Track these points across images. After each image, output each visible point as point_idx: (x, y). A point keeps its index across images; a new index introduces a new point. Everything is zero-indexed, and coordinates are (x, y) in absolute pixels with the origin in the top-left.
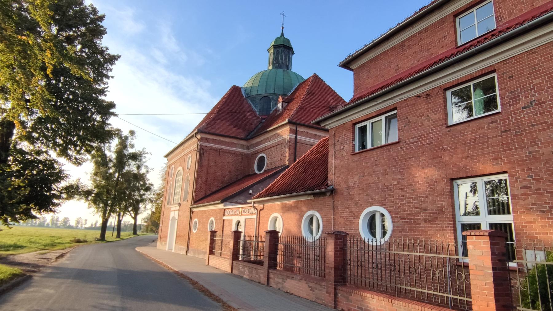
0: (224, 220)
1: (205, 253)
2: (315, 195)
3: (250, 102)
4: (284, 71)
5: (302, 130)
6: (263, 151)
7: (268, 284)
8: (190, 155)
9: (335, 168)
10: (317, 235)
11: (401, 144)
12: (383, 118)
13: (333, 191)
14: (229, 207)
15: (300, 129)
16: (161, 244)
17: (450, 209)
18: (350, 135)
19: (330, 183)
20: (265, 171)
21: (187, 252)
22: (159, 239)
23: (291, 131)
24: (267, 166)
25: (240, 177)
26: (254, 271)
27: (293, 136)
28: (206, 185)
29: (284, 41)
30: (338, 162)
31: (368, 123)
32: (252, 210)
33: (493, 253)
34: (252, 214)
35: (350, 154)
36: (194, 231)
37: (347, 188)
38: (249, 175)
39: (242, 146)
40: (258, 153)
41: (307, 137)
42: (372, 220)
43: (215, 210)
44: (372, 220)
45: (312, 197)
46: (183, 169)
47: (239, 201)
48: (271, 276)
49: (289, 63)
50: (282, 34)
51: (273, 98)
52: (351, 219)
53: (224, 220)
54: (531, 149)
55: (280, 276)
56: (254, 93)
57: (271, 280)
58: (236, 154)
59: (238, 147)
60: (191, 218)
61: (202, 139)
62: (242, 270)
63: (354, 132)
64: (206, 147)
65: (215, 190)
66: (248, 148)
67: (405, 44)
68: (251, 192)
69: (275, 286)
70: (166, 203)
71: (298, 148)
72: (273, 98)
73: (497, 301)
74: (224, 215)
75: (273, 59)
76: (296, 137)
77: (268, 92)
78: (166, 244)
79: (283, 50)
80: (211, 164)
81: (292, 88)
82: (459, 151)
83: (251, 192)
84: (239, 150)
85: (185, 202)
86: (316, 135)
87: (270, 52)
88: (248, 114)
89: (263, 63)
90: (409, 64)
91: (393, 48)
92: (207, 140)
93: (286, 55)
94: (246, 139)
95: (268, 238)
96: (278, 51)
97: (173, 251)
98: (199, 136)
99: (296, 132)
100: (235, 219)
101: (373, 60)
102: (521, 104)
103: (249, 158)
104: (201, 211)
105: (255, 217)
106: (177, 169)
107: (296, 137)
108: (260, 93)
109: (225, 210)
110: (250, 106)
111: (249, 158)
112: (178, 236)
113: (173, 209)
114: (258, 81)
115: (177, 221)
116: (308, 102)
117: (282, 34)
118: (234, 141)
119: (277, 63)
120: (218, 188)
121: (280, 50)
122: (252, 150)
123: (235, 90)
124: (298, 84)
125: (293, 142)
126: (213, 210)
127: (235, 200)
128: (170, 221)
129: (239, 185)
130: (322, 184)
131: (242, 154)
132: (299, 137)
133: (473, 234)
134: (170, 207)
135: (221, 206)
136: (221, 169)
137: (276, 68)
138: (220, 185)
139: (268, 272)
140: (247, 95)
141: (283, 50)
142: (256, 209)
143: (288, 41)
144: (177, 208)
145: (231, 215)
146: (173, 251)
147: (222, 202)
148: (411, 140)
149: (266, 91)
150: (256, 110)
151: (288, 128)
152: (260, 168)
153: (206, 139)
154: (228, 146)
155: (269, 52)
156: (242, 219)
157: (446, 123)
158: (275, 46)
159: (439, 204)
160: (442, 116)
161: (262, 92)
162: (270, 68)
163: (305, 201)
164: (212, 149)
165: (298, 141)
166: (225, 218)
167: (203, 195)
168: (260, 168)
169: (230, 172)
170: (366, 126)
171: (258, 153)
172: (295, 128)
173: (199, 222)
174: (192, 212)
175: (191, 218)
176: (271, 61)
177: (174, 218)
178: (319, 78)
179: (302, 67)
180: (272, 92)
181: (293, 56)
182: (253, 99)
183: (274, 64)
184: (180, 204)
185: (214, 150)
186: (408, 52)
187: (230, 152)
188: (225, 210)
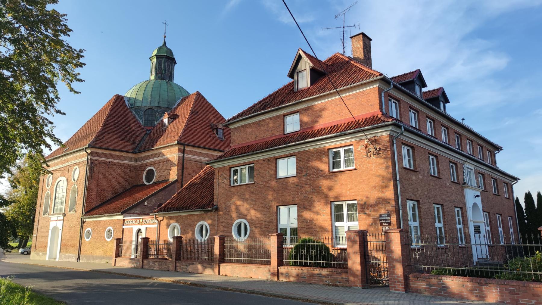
0: (123, 229)
1: (110, 258)
2: (204, 211)
3: (134, 113)
4: (167, 83)
5: (189, 149)
6: (152, 164)
7: (175, 271)
8: (76, 167)
9: (218, 194)
10: (205, 238)
11: (256, 184)
12: (247, 167)
13: (217, 209)
14: (129, 219)
15: (187, 148)
16: (38, 254)
17: (275, 221)
18: (228, 174)
19: (215, 204)
20: (154, 182)
21: (78, 259)
22: (33, 249)
23: (180, 150)
24: (156, 178)
25: (128, 188)
26: (163, 264)
27: (182, 155)
28: (97, 196)
29: (166, 52)
30: (220, 190)
31: (239, 168)
32: (153, 220)
33: (278, 242)
34: (153, 224)
35: (228, 186)
36: (86, 239)
37: (225, 207)
38: (138, 186)
39: (130, 159)
40: (146, 165)
41: (192, 155)
42: (240, 226)
43: (113, 220)
44: (240, 226)
45: (203, 212)
46: (67, 180)
47: (136, 212)
48: (178, 265)
49: (171, 74)
50: (165, 44)
51: (157, 111)
52: (228, 226)
53: (123, 229)
54: (305, 195)
55: (184, 264)
56: (138, 105)
57: (178, 268)
58: (125, 166)
59: (127, 160)
60: (82, 227)
61: (92, 153)
62: (153, 265)
63: (230, 173)
64: (96, 160)
65: (105, 200)
66: (136, 160)
67: (261, 123)
68: (146, 204)
69: (181, 271)
70: (42, 212)
71: (185, 165)
72: (157, 111)
73: (278, 259)
74: (123, 225)
75: (156, 69)
76: (184, 155)
77: (152, 105)
78: (45, 254)
79: (165, 62)
80: (101, 176)
81: (176, 101)
82: (280, 192)
83: (146, 204)
84: (127, 162)
85: (72, 213)
86: (200, 153)
87: (153, 61)
88: (133, 125)
89: (147, 72)
90: (262, 136)
91: (254, 123)
92: (97, 154)
93: (169, 66)
94: (133, 153)
95: (175, 241)
96: (161, 61)
97: (57, 260)
98: (89, 151)
99: (183, 152)
100: (135, 228)
101: (243, 126)
102: (303, 175)
103: (138, 170)
104: (95, 221)
105: (156, 226)
106: (57, 179)
107: (184, 155)
108: (144, 104)
109: (124, 220)
110: (134, 116)
111: (138, 170)
112: (63, 245)
113: (52, 219)
114: (142, 93)
115: (61, 231)
116: (193, 122)
117: (165, 44)
118: (123, 154)
119: (160, 72)
120: (108, 199)
121: (163, 60)
122: (140, 163)
123: (119, 100)
124: (181, 98)
125: (181, 159)
126: (110, 220)
127: (132, 211)
128: (50, 232)
129: (131, 195)
130: (209, 204)
131: (129, 166)
132: (186, 155)
133: (97, 261)
134: (50, 216)
135: (121, 217)
136: (110, 181)
137: (159, 78)
138: (110, 195)
139: (176, 263)
140: (131, 105)
141: (165, 62)
142: (158, 220)
143: (171, 52)
144: (62, 218)
145: (131, 224)
146: (57, 260)
147: (122, 214)
148: (260, 183)
149: (151, 104)
150: (141, 122)
151: (177, 148)
152: (149, 179)
153: (96, 153)
154: (117, 159)
155: (151, 60)
156: (143, 228)
157: (276, 177)
158: (157, 56)
159: (271, 218)
160: (274, 173)
161: (146, 104)
162: (153, 77)
163: (198, 215)
164: (102, 162)
165: (185, 158)
166: (124, 227)
167: (94, 206)
168: (149, 179)
169: (119, 183)
170: (237, 170)
171: (146, 165)
172: (182, 148)
173: (93, 231)
174: (83, 222)
175: (82, 227)
176: (154, 70)
177: (55, 228)
178: (202, 96)
179: (185, 78)
180: (157, 105)
181: (175, 66)
182: (138, 110)
183: (156, 74)
184: (64, 215)
185: (104, 163)
186: (262, 128)
187: (119, 165)
188: (124, 220)
